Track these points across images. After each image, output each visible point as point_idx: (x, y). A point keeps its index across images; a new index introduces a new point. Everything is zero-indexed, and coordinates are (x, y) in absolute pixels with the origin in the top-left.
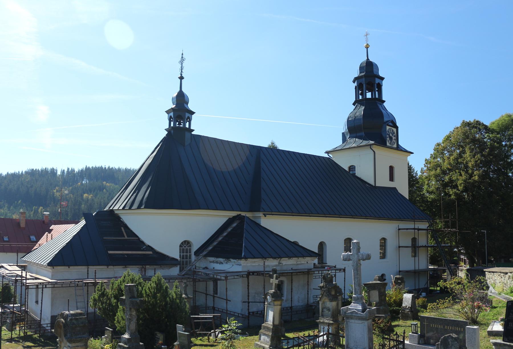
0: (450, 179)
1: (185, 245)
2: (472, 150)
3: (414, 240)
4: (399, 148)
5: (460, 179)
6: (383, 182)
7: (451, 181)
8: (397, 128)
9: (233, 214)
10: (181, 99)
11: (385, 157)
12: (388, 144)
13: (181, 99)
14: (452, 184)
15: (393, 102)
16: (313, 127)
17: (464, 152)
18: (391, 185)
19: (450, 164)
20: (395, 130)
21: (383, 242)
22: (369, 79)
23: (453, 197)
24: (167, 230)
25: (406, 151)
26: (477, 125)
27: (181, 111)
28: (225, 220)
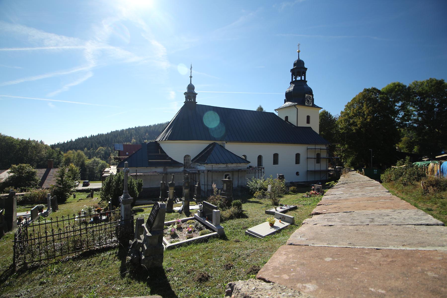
0: (353, 121)
1: (186, 157)
2: (367, 105)
3: (318, 155)
4: (314, 106)
5: (359, 121)
6: (303, 123)
7: (354, 122)
8: (313, 95)
9: (211, 142)
10: (191, 88)
11: (304, 111)
12: (306, 104)
13: (191, 88)
14: (354, 124)
15: (312, 80)
16: (270, 98)
17: (363, 106)
18: (308, 125)
19: (354, 113)
20: (311, 96)
21: (298, 156)
22: (299, 69)
23: (354, 131)
24: (178, 150)
25: (318, 107)
26: (374, 91)
27: (191, 94)
28: (207, 145)
